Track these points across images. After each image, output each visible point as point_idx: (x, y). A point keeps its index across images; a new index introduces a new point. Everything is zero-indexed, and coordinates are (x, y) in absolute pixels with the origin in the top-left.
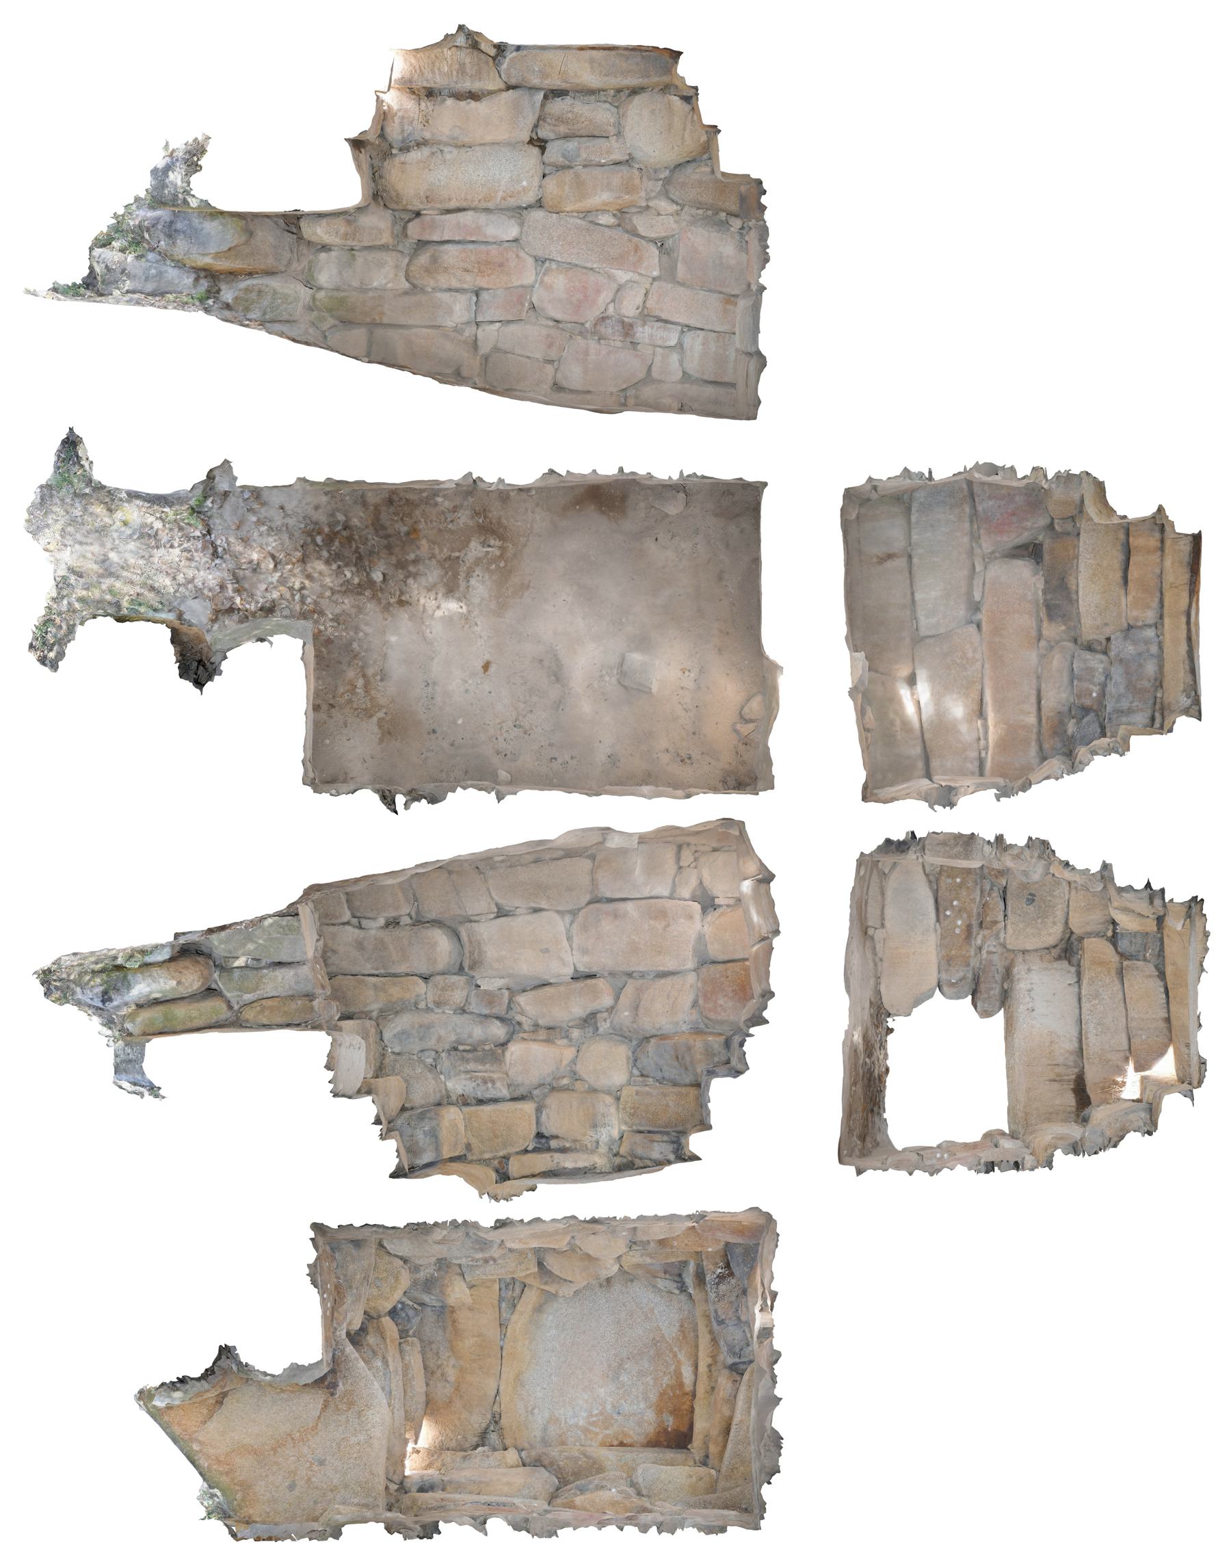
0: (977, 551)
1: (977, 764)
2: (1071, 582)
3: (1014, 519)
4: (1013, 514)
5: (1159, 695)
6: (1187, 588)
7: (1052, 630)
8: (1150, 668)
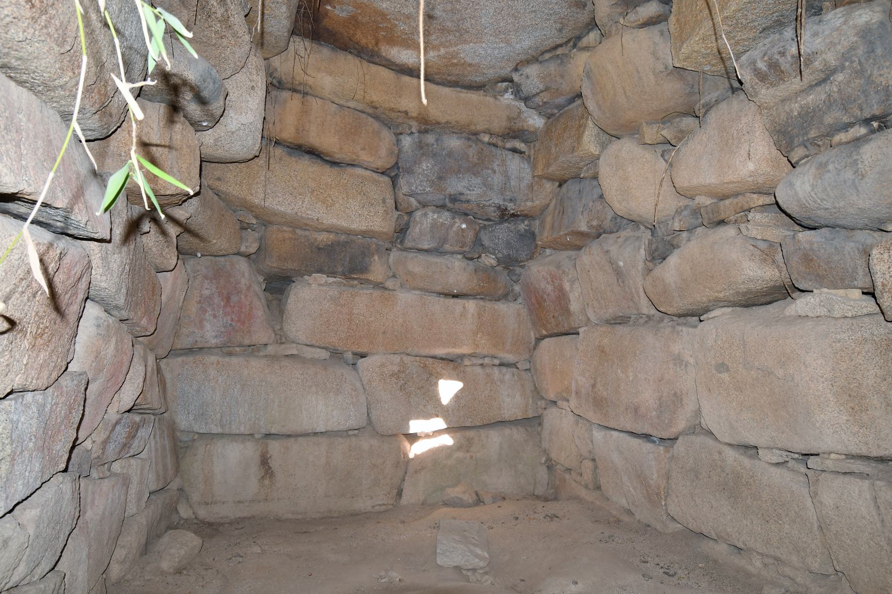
0: (271, 349)
1: (504, 369)
2: (323, 238)
3: (234, 299)
4: (228, 299)
5: (486, 138)
6: (199, 357)
7: (377, 270)
8: (454, 143)
